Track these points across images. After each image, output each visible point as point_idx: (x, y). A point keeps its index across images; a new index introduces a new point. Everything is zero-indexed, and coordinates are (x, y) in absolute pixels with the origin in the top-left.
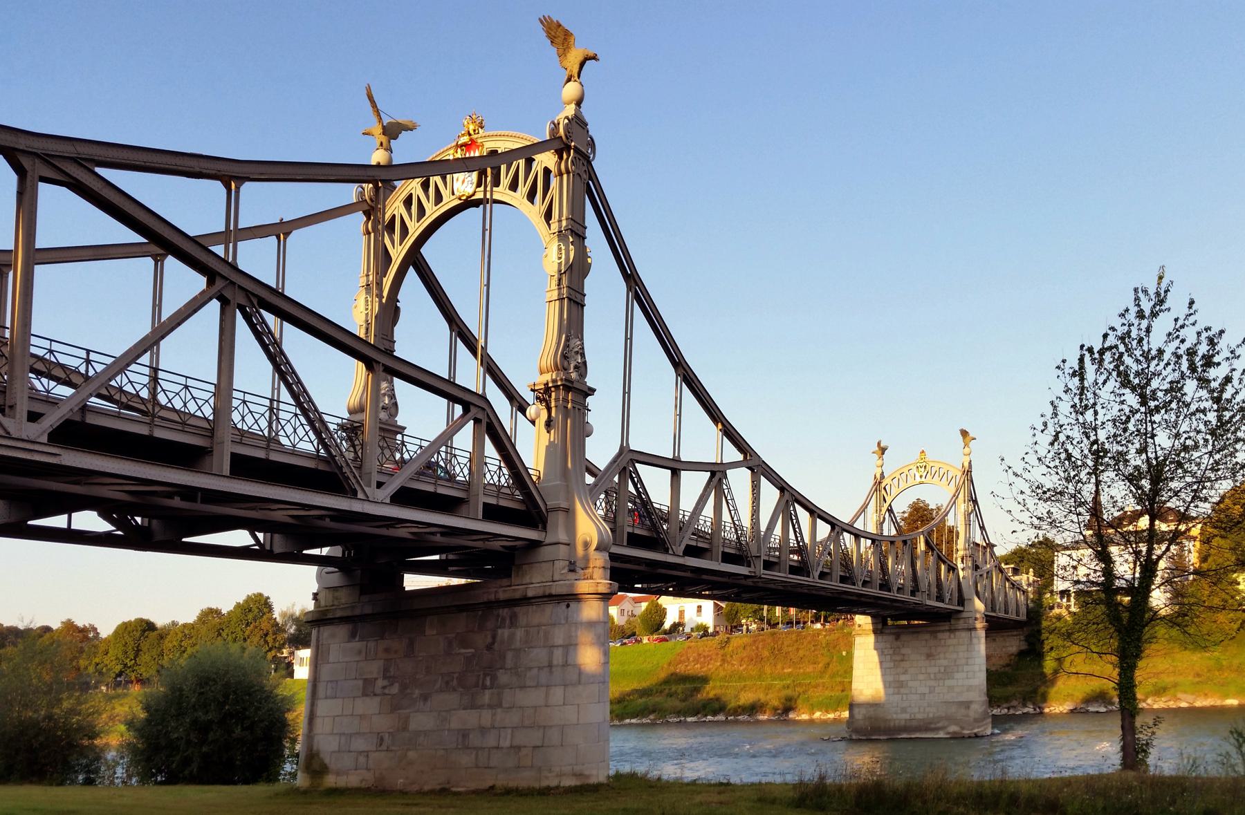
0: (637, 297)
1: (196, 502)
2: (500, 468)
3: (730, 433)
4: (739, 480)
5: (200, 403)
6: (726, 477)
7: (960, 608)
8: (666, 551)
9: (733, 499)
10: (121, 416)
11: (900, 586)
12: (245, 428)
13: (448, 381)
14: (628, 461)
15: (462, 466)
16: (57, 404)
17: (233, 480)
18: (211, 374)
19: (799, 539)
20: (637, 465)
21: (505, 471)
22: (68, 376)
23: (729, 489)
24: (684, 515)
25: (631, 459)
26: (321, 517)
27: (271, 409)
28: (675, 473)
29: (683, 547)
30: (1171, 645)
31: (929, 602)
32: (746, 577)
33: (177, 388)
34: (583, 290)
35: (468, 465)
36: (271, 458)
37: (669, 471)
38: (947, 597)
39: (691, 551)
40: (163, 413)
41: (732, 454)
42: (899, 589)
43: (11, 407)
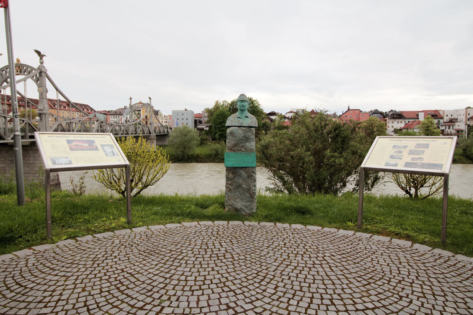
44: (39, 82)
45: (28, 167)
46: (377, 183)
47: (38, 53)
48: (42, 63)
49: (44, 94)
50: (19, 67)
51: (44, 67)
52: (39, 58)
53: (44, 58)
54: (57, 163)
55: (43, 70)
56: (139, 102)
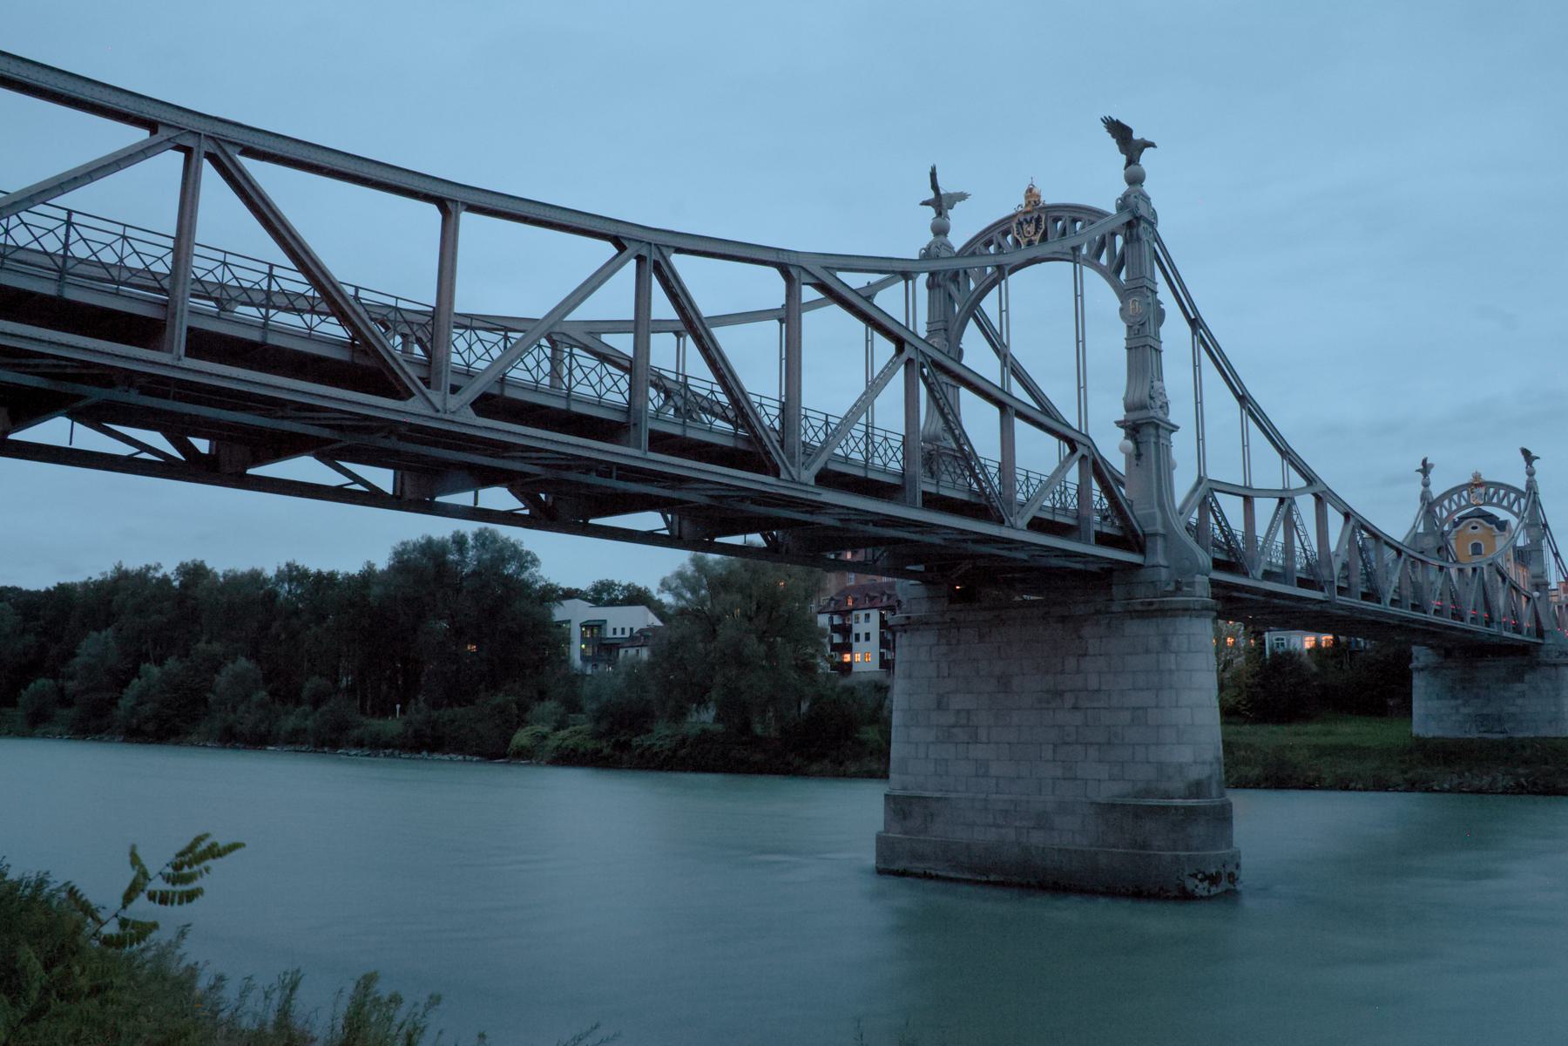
0: (1203, 341)
1: (611, 477)
2: (1101, 498)
3: (1286, 453)
4: (1305, 506)
5: (587, 370)
6: (1294, 503)
7: (1540, 641)
8: (1246, 574)
9: (1302, 525)
10: (312, 337)
11: (1438, 608)
12: (808, 440)
13: (1245, 487)
14: (1206, 493)
15: (895, 450)
16: (473, 376)
17: (1028, 533)
18: (168, 223)
19: (1220, 518)
20: (1216, 493)
21: (1105, 501)
22: (724, 412)
23: (1298, 514)
24: (1277, 546)
25: (1211, 489)
26: (742, 499)
27: (867, 434)
28: (1248, 501)
29: (1028, 518)
30: (958, 606)
31: (1506, 634)
32: (1321, 602)
33: (214, 264)
34: (1159, 337)
35: (901, 448)
36: (869, 476)
37: (1242, 499)
38: (1470, 614)
39: (1268, 575)
40: (81, 269)
41: (1297, 481)
42: (1436, 611)
43: (635, 425)
44: (1123, 276)
45: (1075, 708)
46: (1042, 821)
47: (1119, 131)
48: (1135, 180)
49: (1149, 329)
50: (1038, 220)
51: (1147, 199)
52: (1123, 158)
53: (1147, 159)
54: (984, 739)
55: (1143, 211)
56: (1467, 479)
